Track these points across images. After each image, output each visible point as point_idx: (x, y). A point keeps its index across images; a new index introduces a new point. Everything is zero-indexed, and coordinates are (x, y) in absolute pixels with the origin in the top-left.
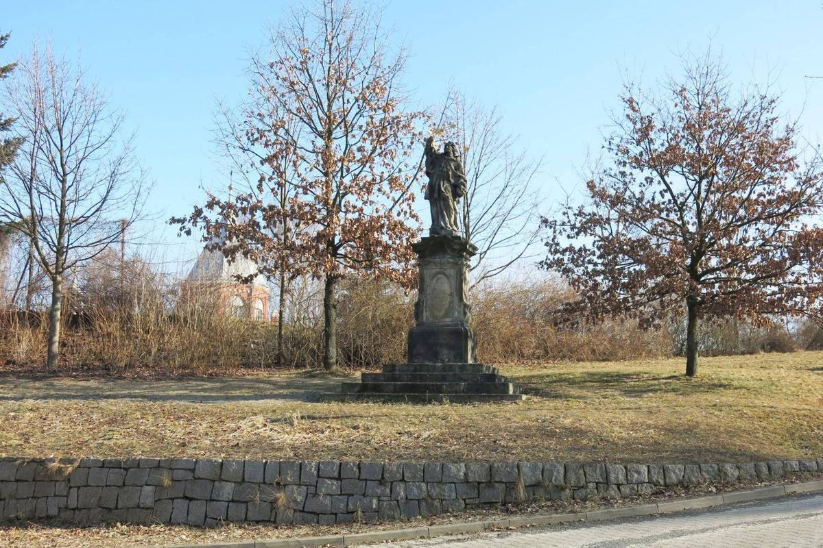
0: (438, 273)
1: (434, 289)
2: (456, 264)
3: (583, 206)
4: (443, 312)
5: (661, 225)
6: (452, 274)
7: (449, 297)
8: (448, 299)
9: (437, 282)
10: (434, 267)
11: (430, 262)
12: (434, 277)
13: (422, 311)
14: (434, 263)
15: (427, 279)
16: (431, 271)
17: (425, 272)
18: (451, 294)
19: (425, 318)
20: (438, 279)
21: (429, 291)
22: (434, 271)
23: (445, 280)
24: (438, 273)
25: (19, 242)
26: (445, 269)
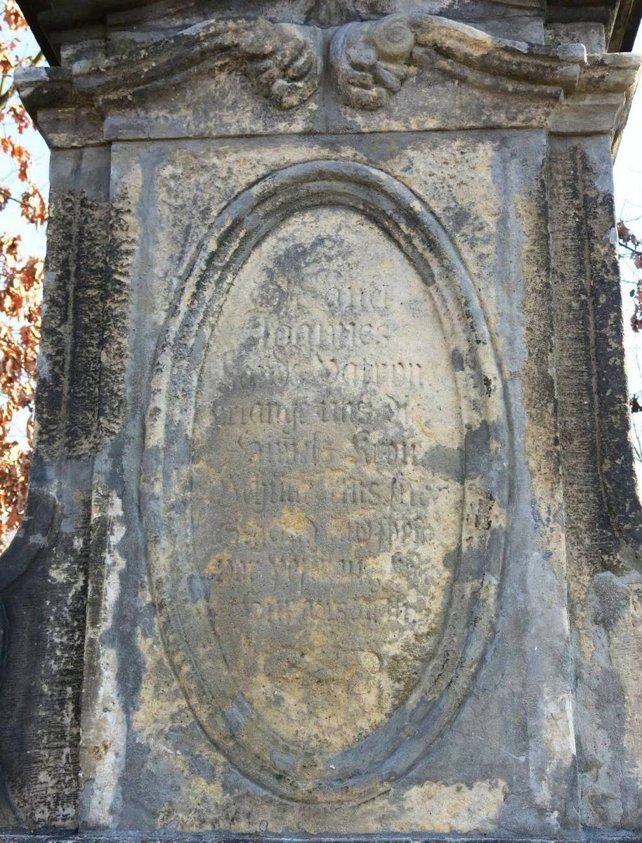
0: (291, 197)
1: (244, 387)
2: (532, 78)
3: (18, 238)
4: (372, 700)
5: (479, 276)
6: (485, 207)
7: (444, 497)
8: (440, 520)
9: (274, 298)
10: (245, 119)
11: (187, 64)
12: (239, 236)
13: (78, 676)
14: (248, 63)
15: (152, 263)
16: (162, 190)
17: (129, 177)
18: (473, 453)
19: (106, 772)
20: (292, 261)
21: (171, 410)
22: (243, 167)
23: (383, 270)
24: (291, 197)
25: (114, 821)
26: (382, 147)
